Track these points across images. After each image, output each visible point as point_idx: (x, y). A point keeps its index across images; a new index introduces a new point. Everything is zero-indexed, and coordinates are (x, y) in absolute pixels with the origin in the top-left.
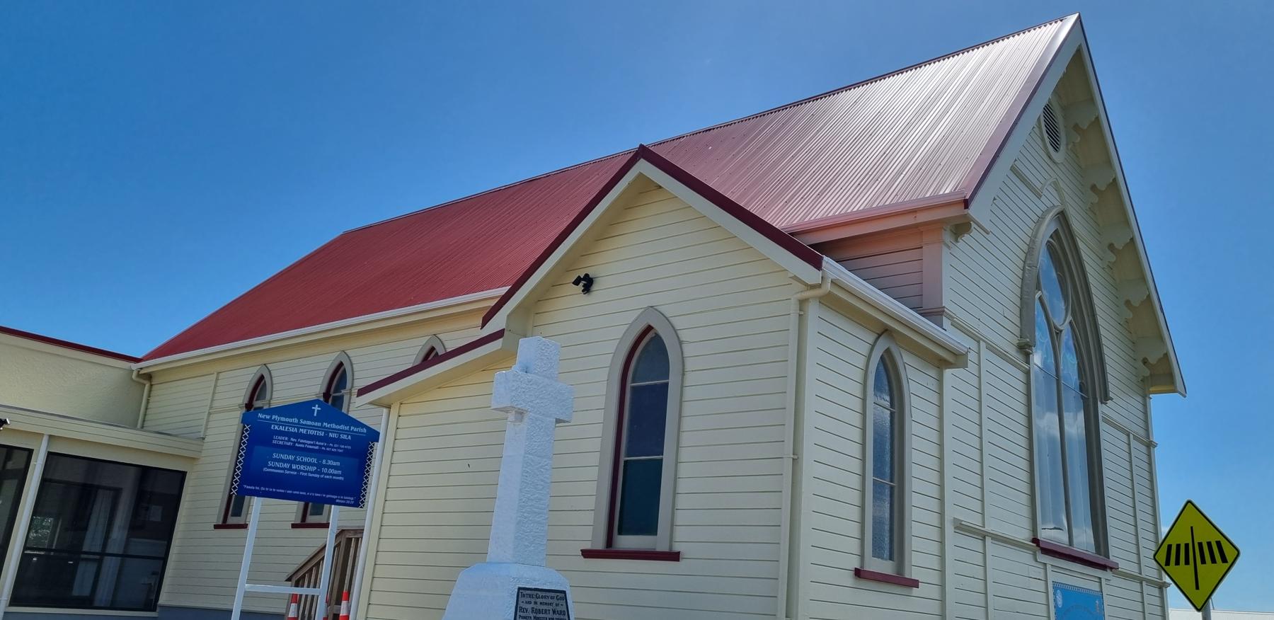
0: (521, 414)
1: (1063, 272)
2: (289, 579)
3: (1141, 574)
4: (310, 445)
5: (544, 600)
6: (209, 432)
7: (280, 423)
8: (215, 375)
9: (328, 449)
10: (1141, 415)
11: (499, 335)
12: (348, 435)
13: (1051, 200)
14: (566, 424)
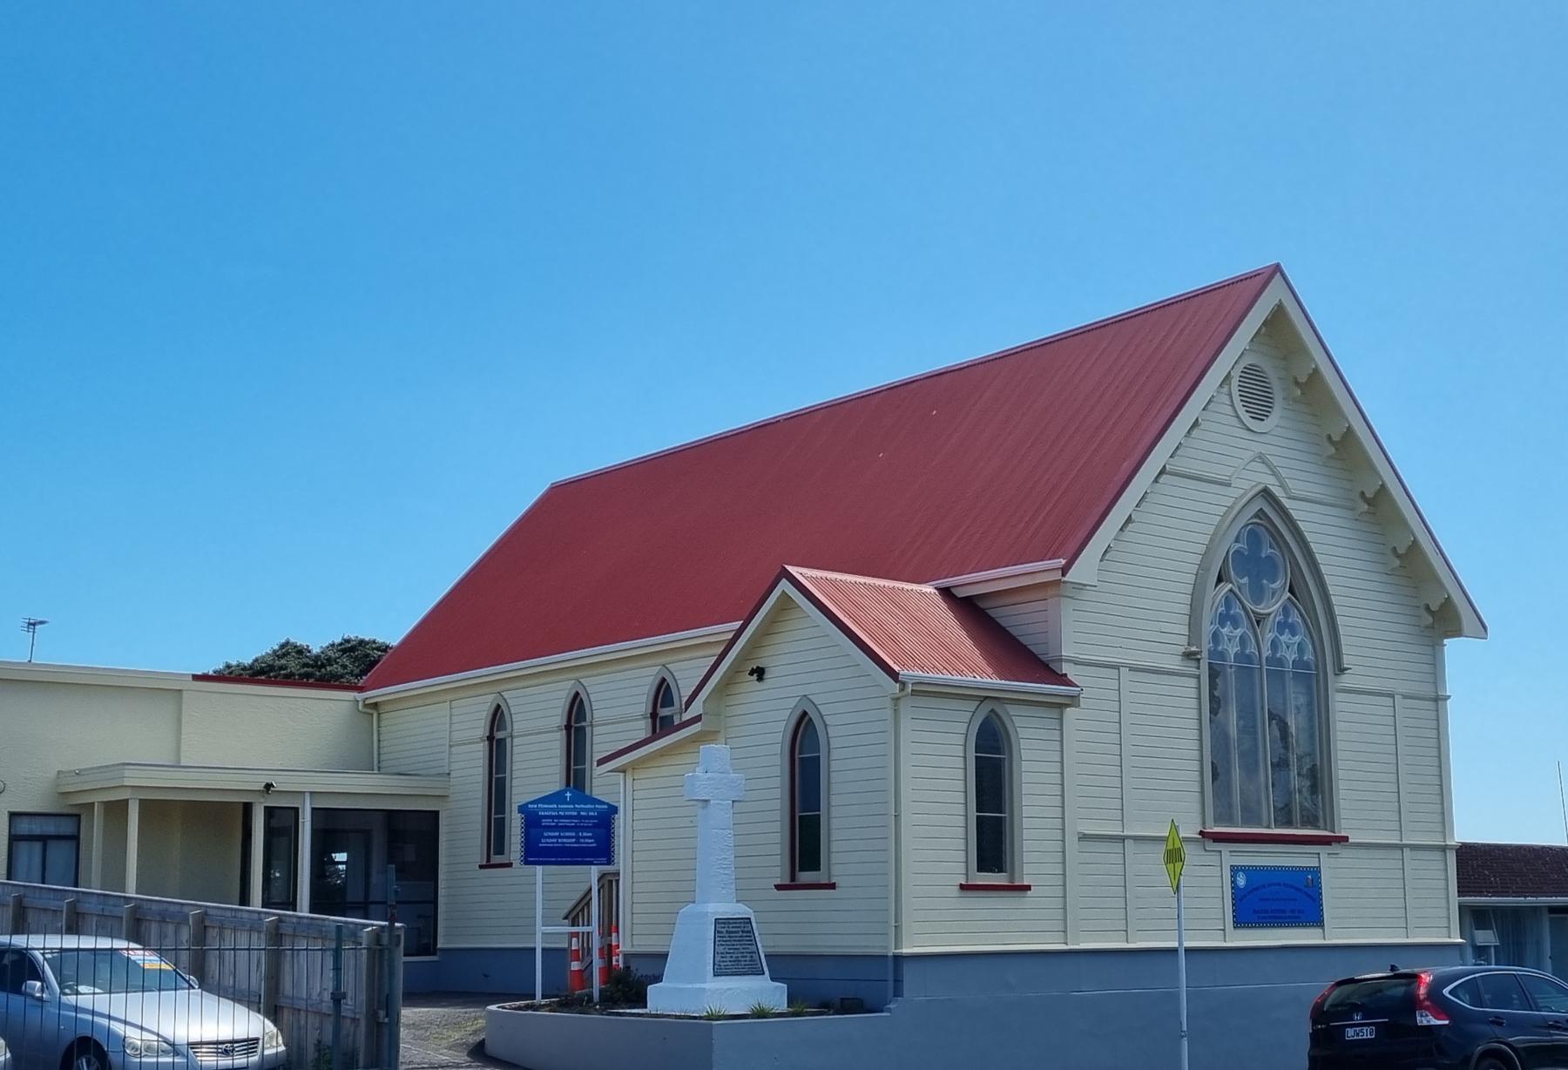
2: (566, 918)
6: (454, 766)
7: (546, 810)
11: (697, 719)
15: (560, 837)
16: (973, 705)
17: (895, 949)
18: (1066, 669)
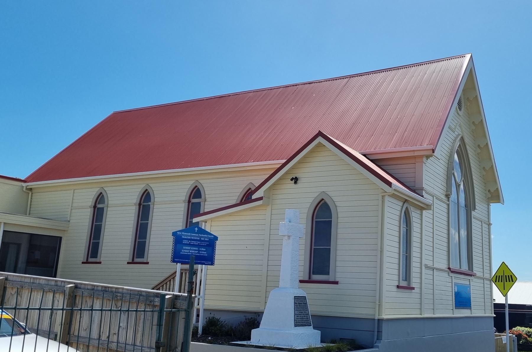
0: (289, 237)
1: (461, 160)
3: (484, 276)
4: (195, 243)
5: (301, 300)
8: (72, 191)
9: (201, 244)
10: (486, 213)
11: (261, 199)
12: (207, 238)
13: (458, 131)
14: (301, 239)
15: (191, 250)
17: (378, 316)
18: (424, 193)
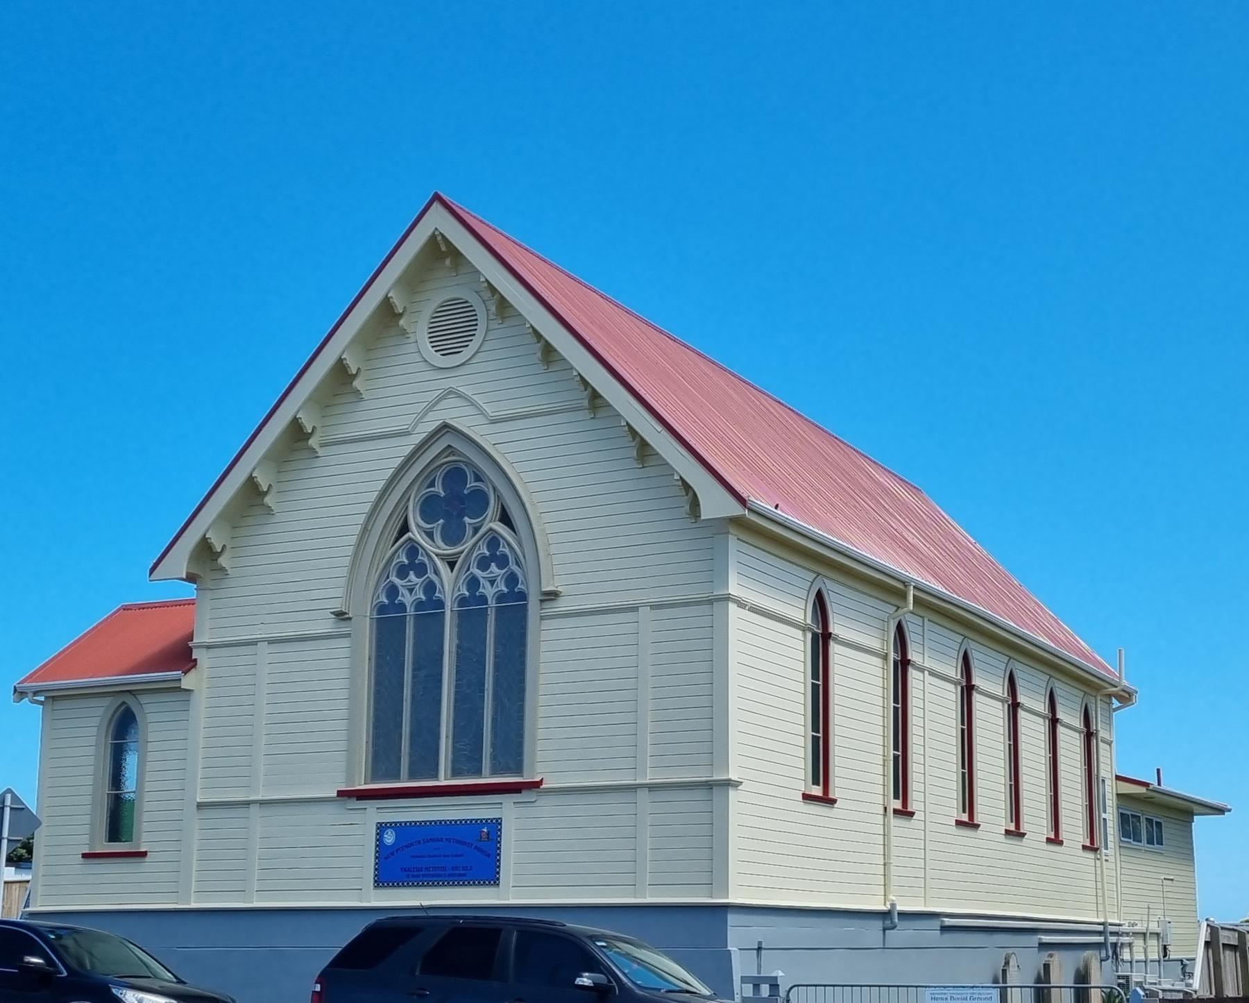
16: (107, 701)
18: (333, 616)
